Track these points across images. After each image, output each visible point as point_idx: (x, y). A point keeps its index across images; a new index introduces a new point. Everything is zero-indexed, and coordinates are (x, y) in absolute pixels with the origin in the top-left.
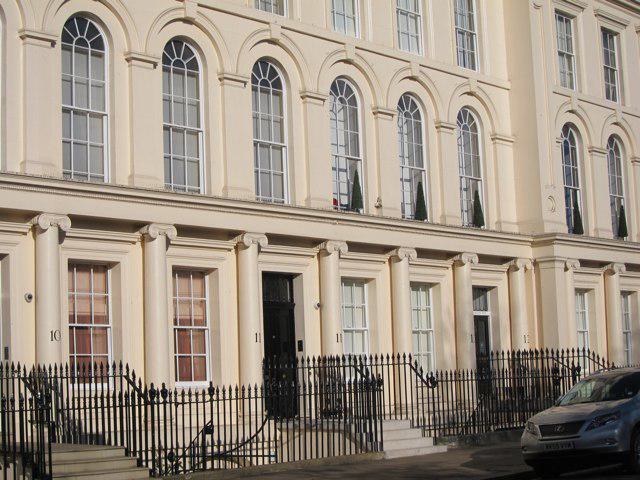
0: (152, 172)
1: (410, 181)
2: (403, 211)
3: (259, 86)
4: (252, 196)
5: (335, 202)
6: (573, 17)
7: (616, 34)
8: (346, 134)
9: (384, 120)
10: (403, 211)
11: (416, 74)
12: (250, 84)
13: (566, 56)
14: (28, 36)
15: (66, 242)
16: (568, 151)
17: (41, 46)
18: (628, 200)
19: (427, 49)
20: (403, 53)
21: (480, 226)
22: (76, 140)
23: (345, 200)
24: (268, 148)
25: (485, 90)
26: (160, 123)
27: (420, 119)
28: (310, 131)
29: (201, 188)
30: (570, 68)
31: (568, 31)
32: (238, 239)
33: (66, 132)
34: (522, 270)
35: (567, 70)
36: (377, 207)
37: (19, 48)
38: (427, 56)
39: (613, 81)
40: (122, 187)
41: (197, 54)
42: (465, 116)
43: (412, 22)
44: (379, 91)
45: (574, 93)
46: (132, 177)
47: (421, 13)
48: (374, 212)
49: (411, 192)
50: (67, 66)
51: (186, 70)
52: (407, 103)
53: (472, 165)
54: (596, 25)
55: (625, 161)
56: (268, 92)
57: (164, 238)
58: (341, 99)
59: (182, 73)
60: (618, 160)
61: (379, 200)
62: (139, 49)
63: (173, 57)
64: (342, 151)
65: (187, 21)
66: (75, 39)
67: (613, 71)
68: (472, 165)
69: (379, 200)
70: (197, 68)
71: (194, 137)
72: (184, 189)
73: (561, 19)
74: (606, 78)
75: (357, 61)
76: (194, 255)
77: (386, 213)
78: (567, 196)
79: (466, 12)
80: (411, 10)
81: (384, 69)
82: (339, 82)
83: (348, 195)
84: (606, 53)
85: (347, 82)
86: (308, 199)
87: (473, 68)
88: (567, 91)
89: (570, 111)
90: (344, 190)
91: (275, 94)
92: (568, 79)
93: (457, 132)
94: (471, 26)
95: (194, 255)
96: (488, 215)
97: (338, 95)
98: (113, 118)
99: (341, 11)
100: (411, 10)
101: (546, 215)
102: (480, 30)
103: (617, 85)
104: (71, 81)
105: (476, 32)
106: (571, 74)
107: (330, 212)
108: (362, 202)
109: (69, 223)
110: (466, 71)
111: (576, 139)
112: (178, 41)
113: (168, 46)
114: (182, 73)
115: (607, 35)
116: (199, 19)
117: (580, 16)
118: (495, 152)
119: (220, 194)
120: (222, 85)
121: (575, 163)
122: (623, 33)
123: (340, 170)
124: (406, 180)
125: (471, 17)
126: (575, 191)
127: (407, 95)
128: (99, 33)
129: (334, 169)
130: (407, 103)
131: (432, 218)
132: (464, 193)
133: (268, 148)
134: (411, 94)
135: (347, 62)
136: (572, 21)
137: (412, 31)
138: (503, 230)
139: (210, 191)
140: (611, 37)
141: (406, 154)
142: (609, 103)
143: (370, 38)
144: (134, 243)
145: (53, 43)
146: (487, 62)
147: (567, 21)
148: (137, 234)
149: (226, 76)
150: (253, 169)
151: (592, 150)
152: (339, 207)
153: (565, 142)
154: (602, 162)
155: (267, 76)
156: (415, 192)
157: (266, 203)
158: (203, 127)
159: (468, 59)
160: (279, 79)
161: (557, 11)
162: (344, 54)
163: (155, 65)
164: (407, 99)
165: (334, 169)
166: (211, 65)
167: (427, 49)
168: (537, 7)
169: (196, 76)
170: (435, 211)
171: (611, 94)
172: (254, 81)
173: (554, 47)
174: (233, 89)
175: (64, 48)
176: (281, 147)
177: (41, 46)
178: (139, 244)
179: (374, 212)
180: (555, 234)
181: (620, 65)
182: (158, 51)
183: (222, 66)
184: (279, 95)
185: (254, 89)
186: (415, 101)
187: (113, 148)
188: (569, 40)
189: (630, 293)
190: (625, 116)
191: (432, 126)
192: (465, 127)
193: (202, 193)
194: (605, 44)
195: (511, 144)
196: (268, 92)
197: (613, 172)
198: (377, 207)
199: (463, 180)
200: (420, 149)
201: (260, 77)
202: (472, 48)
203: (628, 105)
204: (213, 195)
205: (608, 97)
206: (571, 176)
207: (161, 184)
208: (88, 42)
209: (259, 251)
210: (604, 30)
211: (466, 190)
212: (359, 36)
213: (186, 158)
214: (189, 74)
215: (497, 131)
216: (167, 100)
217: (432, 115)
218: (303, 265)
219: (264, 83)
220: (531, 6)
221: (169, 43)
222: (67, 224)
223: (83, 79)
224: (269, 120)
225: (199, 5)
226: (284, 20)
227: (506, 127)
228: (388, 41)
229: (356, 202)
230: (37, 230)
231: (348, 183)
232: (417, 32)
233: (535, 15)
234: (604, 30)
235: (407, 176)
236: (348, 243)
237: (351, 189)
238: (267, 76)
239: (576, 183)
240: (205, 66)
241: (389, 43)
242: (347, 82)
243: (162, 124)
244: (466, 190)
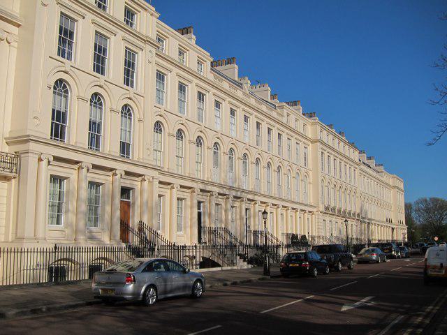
12: (89, 102)
32: (114, 172)
34: (147, 180)
41: (68, 88)
65: (65, 72)
70: (131, 116)
76: (60, 170)
81: (241, 146)
91: (65, 96)
95: (60, 170)
112: (96, 94)
113: (56, 82)
127: (126, 106)
129: (197, 162)
131: (69, 140)
134: (161, 122)
172: (91, 101)
180: (28, 136)
181: (76, 39)
184: (130, 119)
185: (91, 105)
189: (162, 196)
205: (94, 70)
209: (88, 172)
218: (136, 184)
219: (95, 103)
221: (57, 81)
222: (51, 159)
228: (176, 110)
236: (93, 165)
240: (71, 92)
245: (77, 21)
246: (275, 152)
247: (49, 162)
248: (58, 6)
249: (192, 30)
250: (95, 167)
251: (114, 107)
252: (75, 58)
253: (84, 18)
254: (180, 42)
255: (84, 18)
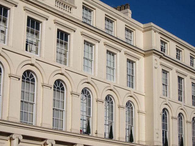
0: (48, 122)
1: (108, 125)
2: (105, 135)
3: (56, 89)
4: (51, 127)
5: (81, 131)
6: (168, 72)
7: (183, 79)
8: (109, 113)
9: (100, 104)
10: (105, 135)
11: (112, 88)
13: (165, 85)
14: (44, 85)
15: (20, 143)
16: (164, 118)
17: (15, 80)
18: (184, 135)
19: (94, 71)
20: (108, 81)
21: (132, 142)
22: (30, 112)
23: (85, 131)
24: (58, 111)
25: (39, 63)
26: (20, 99)
27: (90, 98)
28: (74, 106)
29: (33, 123)
30: (166, 90)
31: (166, 77)
32: (45, 141)
33: (22, 108)
35: (165, 90)
36: (96, 133)
37: (8, 79)
38: (116, 83)
39: (181, 95)
40: (38, 127)
41: (35, 77)
42: (129, 104)
43: (90, 62)
44: (99, 93)
45: (167, 98)
46: (8, 117)
47: (115, 68)
48: (95, 135)
49: (108, 129)
50: (23, 87)
51: (30, 82)
52: (109, 98)
53: (131, 121)
54: (176, 75)
55: (169, 117)
56: (59, 91)
57: (18, 139)
58: (85, 96)
59: (29, 83)
60: (182, 122)
61: (97, 131)
62: (14, 73)
63: (26, 77)
64: (85, 114)
65: (62, 74)
66: (27, 77)
67: (181, 91)
68: (131, 121)
69: (97, 131)
70: (34, 81)
71: (62, 112)
72: (27, 123)
73: (164, 73)
74: (179, 94)
75: (114, 90)
77: (99, 136)
78: (163, 133)
79: (131, 68)
80: (112, 66)
82: (85, 90)
83: (86, 129)
84: (179, 85)
85: (87, 90)
86: (71, 129)
87: (133, 88)
88: (165, 97)
89: (181, 109)
90: (85, 127)
92: (166, 93)
93: (126, 110)
94: (133, 74)
96: (135, 138)
97: (84, 94)
98: (37, 104)
99: (87, 65)
100: (112, 66)
101: (155, 139)
102: (136, 74)
103: (183, 96)
104: (24, 92)
105: (134, 75)
106: (166, 92)
107: (78, 134)
108: (133, 139)
109: (22, 137)
110: (130, 89)
111: (167, 114)
112: (28, 71)
113: (24, 73)
114: (29, 83)
115: (180, 79)
116: (36, 65)
117: (171, 72)
118: (139, 116)
119: (69, 131)
120: (97, 103)
121: (166, 122)
122: (185, 78)
123: (83, 120)
124: (107, 125)
125: (133, 70)
126: (166, 132)
127: (108, 96)
128: (63, 85)
129: (81, 119)
130: (109, 98)
131: (92, 134)
132: (127, 130)
133: (58, 111)
135: (88, 83)
136: (168, 73)
137: (112, 74)
138: (140, 144)
139: (66, 130)
140: (181, 80)
141: (107, 116)
142: (180, 102)
143: (97, 75)
144: (7, 140)
145: (19, 79)
146: (137, 86)
147: (166, 73)
148: (9, 137)
149: (44, 85)
150: (52, 118)
151: (187, 122)
152: (82, 133)
153: (163, 115)
154: (176, 122)
155: (59, 86)
156: (110, 129)
157: (55, 129)
158: (35, 102)
159: (131, 84)
160: (63, 87)
161: (163, 70)
162: (30, 61)
163: (19, 79)
164: (109, 97)
165: (81, 119)
166: (39, 80)
167: (94, 71)
168: (156, 68)
169: (34, 84)
170: (116, 136)
171: (180, 99)
172: (54, 87)
173: (161, 82)
174: (47, 90)
175: (22, 81)
176: (63, 111)
177: (15, 80)
178: (9, 141)
179: (95, 135)
182: (21, 74)
183: (43, 81)
184: (63, 93)
185: (54, 90)
186: (131, 103)
187: (36, 114)
188: (166, 80)
190: (185, 107)
191: (117, 107)
192: (128, 108)
193: (33, 125)
194: (179, 82)
195: (144, 114)
196: (59, 91)
197: (180, 126)
198: (96, 133)
199: (127, 126)
200: (112, 115)
201: (57, 86)
202: (133, 81)
203: (186, 103)
204: (3, 119)
205: (179, 100)
206: (165, 126)
207: (18, 120)
208: (60, 88)
210: (179, 77)
211: (128, 129)
212: (93, 74)
213: (23, 111)
214: (31, 83)
215: (140, 110)
216: (23, 92)
217: (137, 108)
219: (58, 88)
220: (154, 67)
221: (25, 72)
222: (21, 138)
223: (28, 91)
224: (59, 101)
225: (36, 60)
226: (66, 67)
227: (143, 108)
228: (80, 68)
229: (88, 132)
230: (11, 139)
231: (86, 124)
232: (113, 74)
233: (155, 71)
234: (179, 77)
235: (107, 124)
236: (55, 141)
237: (87, 127)
238: (59, 86)
239: (166, 129)
241: (103, 77)
242: (87, 90)
243: (20, 100)
244: (128, 129)
245: (94, 45)
246: (121, 78)
247: (19, 141)
248: (104, 46)
249: (129, 7)
250: (25, 137)
251: (99, 98)
252: (8, 40)
253: (75, 31)
254: (126, 22)
255: (75, 31)
